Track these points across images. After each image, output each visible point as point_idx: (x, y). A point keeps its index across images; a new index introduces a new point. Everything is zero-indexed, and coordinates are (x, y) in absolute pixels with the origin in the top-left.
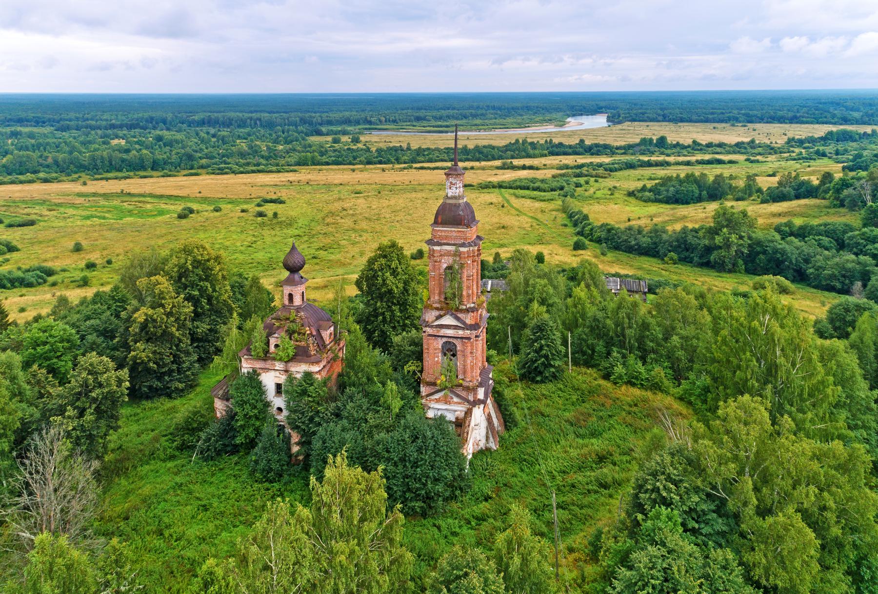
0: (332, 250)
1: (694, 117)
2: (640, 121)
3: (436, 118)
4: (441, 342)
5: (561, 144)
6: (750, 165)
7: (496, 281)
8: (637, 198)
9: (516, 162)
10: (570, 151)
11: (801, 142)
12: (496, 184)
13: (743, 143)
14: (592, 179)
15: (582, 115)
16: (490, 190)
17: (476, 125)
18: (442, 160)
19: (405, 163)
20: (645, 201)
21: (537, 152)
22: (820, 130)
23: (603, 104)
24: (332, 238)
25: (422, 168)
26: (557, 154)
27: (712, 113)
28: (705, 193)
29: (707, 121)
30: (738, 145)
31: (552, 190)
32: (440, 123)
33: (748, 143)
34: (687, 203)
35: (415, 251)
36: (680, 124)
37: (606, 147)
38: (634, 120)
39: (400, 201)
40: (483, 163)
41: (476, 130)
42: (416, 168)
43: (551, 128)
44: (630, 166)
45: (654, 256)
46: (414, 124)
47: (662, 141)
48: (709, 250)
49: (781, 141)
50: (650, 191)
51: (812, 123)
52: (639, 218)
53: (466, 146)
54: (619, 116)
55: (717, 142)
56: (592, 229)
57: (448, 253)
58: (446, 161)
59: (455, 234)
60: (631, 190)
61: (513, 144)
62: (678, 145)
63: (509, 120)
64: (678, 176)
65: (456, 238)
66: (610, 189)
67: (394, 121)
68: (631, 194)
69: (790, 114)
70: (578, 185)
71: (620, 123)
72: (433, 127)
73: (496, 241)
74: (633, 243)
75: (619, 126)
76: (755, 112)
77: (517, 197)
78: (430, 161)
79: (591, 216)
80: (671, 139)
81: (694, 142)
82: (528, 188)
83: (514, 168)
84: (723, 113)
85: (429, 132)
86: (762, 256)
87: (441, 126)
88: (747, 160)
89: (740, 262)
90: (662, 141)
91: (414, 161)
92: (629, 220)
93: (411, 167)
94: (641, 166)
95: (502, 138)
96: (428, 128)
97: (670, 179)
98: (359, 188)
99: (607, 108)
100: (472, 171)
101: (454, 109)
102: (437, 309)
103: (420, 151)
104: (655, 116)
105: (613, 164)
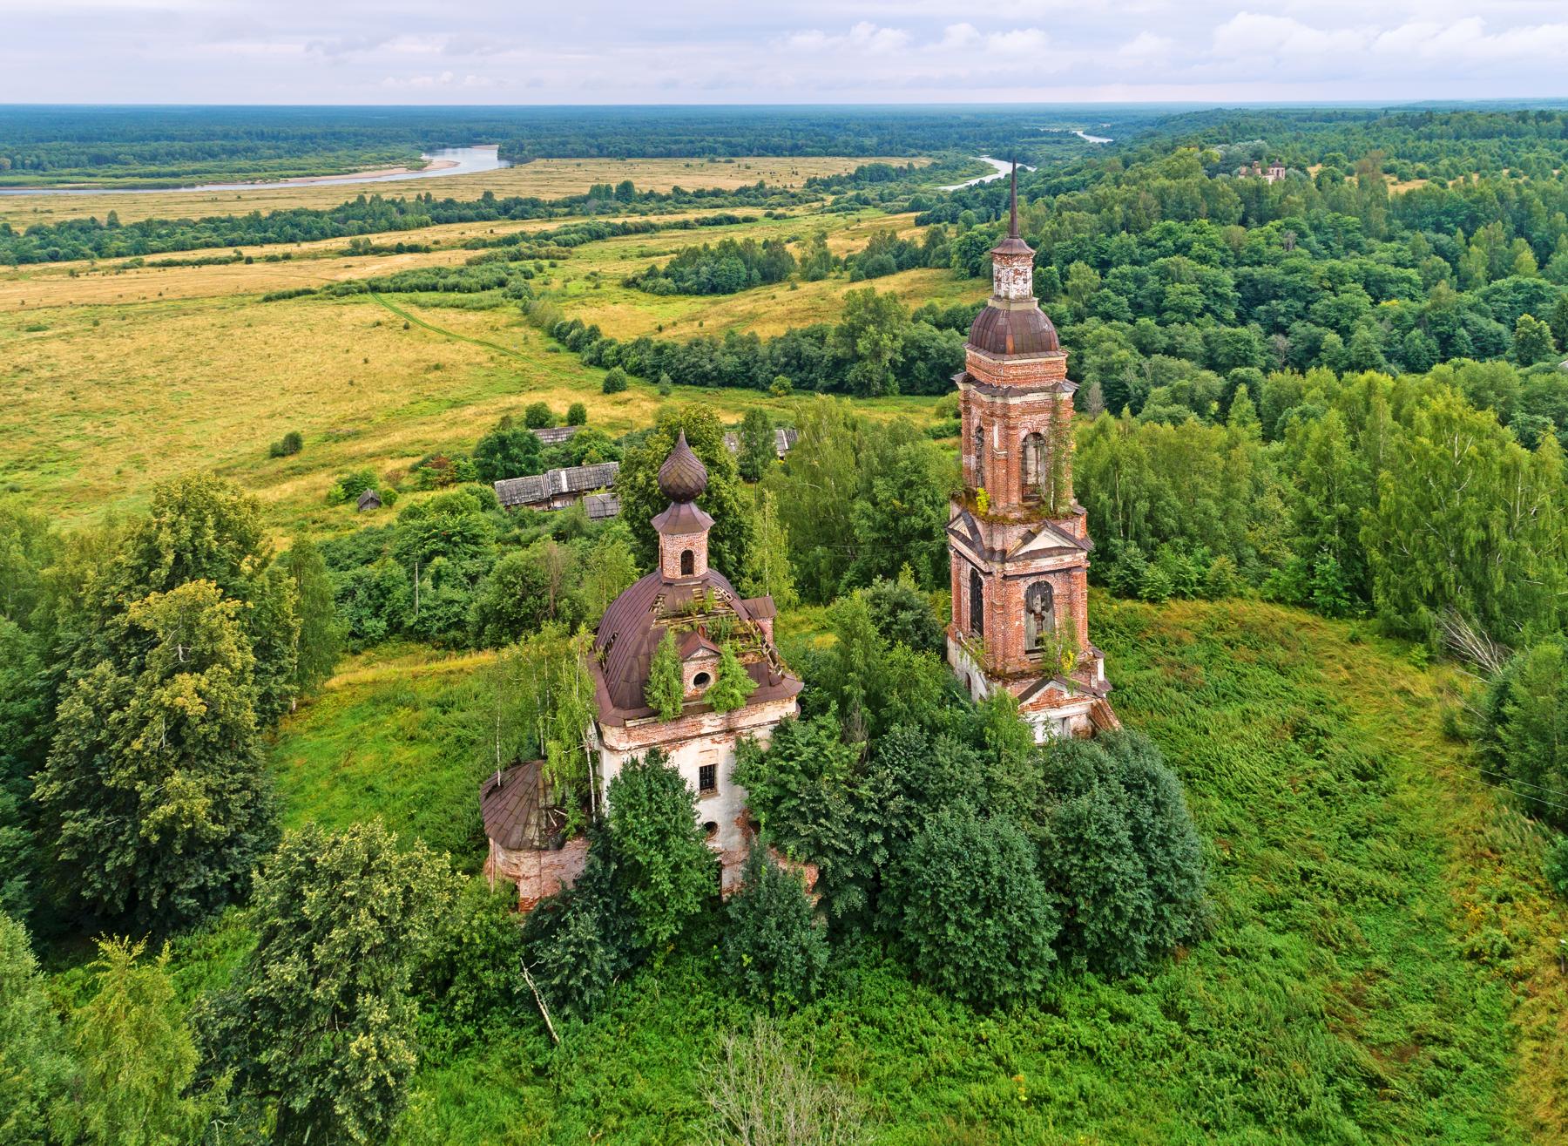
0: (48, 467)
1: (650, 149)
2: (559, 157)
3: (142, 158)
4: (1023, 586)
5: (449, 203)
6: (777, 223)
7: (574, 470)
8: (644, 290)
9: (376, 240)
10: (471, 213)
11: (827, 185)
12: (365, 285)
13: (749, 189)
14: (546, 263)
15: (445, 147)
16: (355, 298)
17: (239, 171)
18: (207, 245)
19: (118, 255)
20: (661, 294)
21: (409, 218)
22: (845, 166)
23: (481, 128)
24: (33, 439)
25: (170, 264)
26: (448, 221)
27: (676, 142)
28: (755, 272)
29: (669, 154)
30: (742, 191)
31: (484, 288)
32: (154, 169)
33: (756, 189)
34: (732, 291)
35: (279, 438)
36: (629, 161)
37: (535, 203)
38: (549, 156)
39: (164, 336)
40: (305, 246)
41: (244, 181)
42: (153, 265)
43: (401, 174)
44: (598, 236)
45: (745, 386)
46: (91, 171)
47: (626, 190)
48: (839, 364)
49: (798, 185)
50: (666, 275)
51: (819, 155)
52: (675, 324)
53: (257, 213)
54: (522, 148)
55: (710, 189)
56: (618, 352)
57: (1030, 409)
58: (216, 245)
59: (1041, 370)
60: (630, 277)
61: (352, 205)
62: (651, 196)
63: (310, 160)
64: (706, 247)
65: (1045, 376)
66: (587, 278)
67: (37, 167)
68: (630, 284)
69: (789, 143)
70: (528, 275)
71: (524, 161)
72: (141, 176)
73: (437, 395)
74: (709, 367)
75: (529, 167)
76: (740, 140)
77: (423, 306)
78: (181, 247)
79: (603, 328)
80: (641, 186)
81: (676, 189)
82: (435, 288)
83: (378, 251)
84: (691, 142)
85: (134, 187)
86: (921, 364)
87: (159, 175)
88: (769, 215)
89: (892, 377)
90: (626, 190)
91: (140, 250)
92: (660, 329)
93: (141, 264)
94: (613, 234)
95: (329, 192)
96: (727, 177)
97: (694, 254)
98: (32, 317)
99: (503, 135)
100: (289, 263)
101: (172, 138)
102: (1020, 521)
103: (146, 229)
104: (584, 147)
105: (566, 233)
